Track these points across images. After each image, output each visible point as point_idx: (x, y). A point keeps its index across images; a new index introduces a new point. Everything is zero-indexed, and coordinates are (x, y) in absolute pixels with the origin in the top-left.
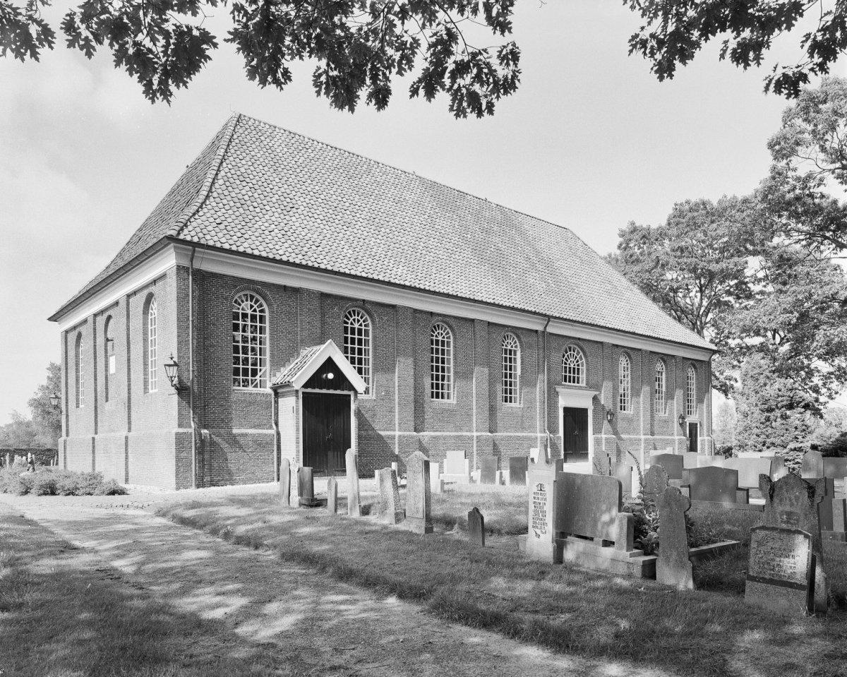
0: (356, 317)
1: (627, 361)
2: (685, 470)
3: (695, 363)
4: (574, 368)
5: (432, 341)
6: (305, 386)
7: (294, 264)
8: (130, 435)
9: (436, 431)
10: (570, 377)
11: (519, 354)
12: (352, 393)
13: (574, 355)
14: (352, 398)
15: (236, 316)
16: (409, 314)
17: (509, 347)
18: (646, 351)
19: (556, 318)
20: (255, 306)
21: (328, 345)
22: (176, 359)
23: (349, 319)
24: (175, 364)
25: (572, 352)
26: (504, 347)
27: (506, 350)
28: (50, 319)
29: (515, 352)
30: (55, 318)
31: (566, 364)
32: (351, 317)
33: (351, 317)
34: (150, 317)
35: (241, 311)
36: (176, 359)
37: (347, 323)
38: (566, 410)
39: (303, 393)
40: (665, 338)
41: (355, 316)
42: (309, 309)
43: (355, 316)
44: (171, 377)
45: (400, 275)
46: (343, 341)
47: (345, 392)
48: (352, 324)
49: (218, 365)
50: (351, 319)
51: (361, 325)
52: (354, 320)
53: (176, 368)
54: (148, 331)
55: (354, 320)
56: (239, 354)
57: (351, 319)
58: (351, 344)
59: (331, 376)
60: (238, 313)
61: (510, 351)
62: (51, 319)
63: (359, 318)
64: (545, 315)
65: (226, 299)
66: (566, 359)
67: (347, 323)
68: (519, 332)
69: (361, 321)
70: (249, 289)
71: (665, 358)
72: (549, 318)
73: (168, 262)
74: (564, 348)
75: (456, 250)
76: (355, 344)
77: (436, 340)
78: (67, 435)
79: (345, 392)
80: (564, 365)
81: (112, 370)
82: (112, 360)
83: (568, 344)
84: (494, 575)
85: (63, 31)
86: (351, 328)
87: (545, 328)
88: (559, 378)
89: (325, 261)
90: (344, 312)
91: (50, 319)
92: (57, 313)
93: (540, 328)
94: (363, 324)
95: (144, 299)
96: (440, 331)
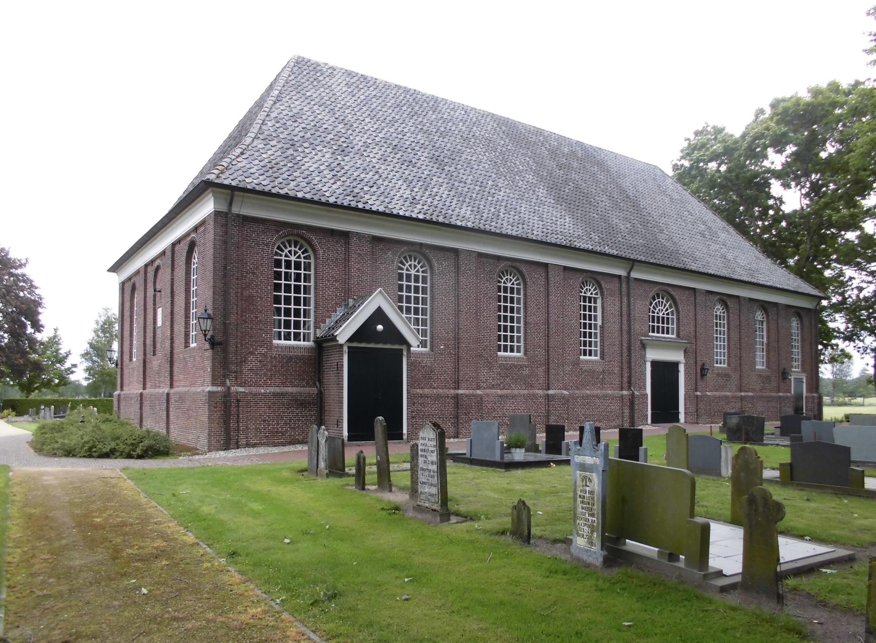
0: (509, 277)
1: (763, 315)
2: (353, 476)
3: (799, 312)
4: (663, 318)
5: (499, 287)
6: (351, 340)
7: (342, 207)
8: (145, 392)
9: (504, 388)
10: (658, 327)
11: (599, 302)
12: (404, 347)
13: (662, 302)
14: (405, 353)
15: (278, 263)
16: (562, 269)
17: (588, 294)
18: (744, 298)
19: (640, 262)
20: (300, 252)
21: (378, 293)
22: (210, 312)
23: (404, 265)
24: (209, 317)
25: (661, 300)
26: (583, 294)
27: (585, 298)
28: (110, 270)
29: (595, 299)
30: (115, 268)
31: (653, 312)
32: (407, 262)
33: (286, 248)
34: (193, 267)
35: (283, 258)
36: (210, 312)
37: (403, 269)
38: (655, 364)
39: (349, 347)
40: (766, 283)
41: (411, 261)
42: (359, 255)
43: (411, 261)
44: (205, 331)
45: (464, 215)
46: (396, 288)
47: (396, 347)
48: (407, 270)
49: (256, 318)
50: (407, 265)
51: (418, 271)
52: (410, 266)
53: (209, 321)
54: (190, 281)
55: (410, 266)
56: (281, 304)
57: (407, 265)
58: (591, 306)
59: (380, 327)
60: (281, 260)
61: (590, 298)
62: (110, 270)
63: (416, 263)
64: (629, 259)
65: (267, 245)
66: (654, 307)
67: (403, 269)
68: (599, 278)
69: (419, 266)
70: (293, 235)
71: (766, 306)
72: (632, 263)
73: (207, 208)
74: (651, 295)
75: (582, 198)
76: (411, 293)
77: (504, 287)
78: (122, 389)
79: (396, 347)
80: (651, 314)
81: (159, 323)
82: (160, 311)
83: (655, 290)
84: (580, 548)
85: (686, 144)
86: (504, 286)
87: (629, 273)
88: (645, 329)
89: (378, 203)
90: (399, 257)
91: (110, 270)
92: (122, 264)
93: (622, 273)
94: (421, 270)
95: (186, 248)
96: (286, 251)
